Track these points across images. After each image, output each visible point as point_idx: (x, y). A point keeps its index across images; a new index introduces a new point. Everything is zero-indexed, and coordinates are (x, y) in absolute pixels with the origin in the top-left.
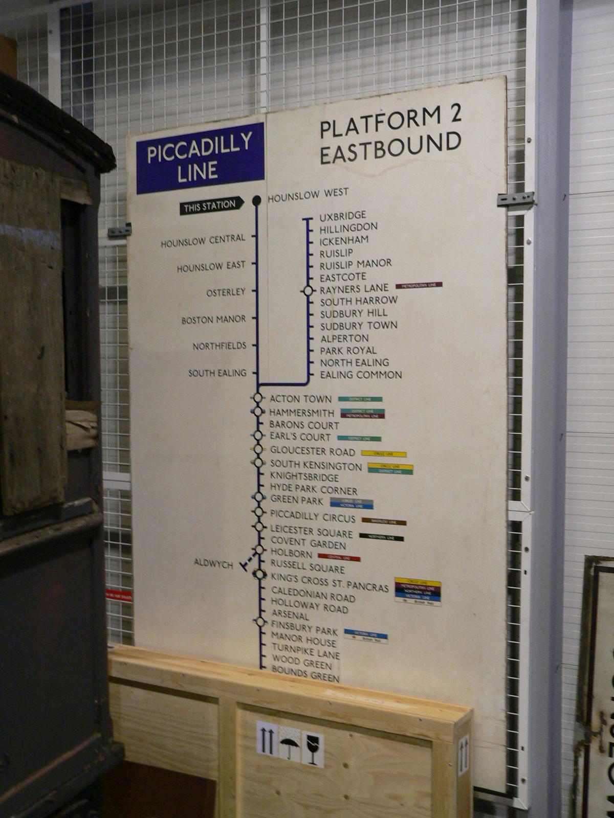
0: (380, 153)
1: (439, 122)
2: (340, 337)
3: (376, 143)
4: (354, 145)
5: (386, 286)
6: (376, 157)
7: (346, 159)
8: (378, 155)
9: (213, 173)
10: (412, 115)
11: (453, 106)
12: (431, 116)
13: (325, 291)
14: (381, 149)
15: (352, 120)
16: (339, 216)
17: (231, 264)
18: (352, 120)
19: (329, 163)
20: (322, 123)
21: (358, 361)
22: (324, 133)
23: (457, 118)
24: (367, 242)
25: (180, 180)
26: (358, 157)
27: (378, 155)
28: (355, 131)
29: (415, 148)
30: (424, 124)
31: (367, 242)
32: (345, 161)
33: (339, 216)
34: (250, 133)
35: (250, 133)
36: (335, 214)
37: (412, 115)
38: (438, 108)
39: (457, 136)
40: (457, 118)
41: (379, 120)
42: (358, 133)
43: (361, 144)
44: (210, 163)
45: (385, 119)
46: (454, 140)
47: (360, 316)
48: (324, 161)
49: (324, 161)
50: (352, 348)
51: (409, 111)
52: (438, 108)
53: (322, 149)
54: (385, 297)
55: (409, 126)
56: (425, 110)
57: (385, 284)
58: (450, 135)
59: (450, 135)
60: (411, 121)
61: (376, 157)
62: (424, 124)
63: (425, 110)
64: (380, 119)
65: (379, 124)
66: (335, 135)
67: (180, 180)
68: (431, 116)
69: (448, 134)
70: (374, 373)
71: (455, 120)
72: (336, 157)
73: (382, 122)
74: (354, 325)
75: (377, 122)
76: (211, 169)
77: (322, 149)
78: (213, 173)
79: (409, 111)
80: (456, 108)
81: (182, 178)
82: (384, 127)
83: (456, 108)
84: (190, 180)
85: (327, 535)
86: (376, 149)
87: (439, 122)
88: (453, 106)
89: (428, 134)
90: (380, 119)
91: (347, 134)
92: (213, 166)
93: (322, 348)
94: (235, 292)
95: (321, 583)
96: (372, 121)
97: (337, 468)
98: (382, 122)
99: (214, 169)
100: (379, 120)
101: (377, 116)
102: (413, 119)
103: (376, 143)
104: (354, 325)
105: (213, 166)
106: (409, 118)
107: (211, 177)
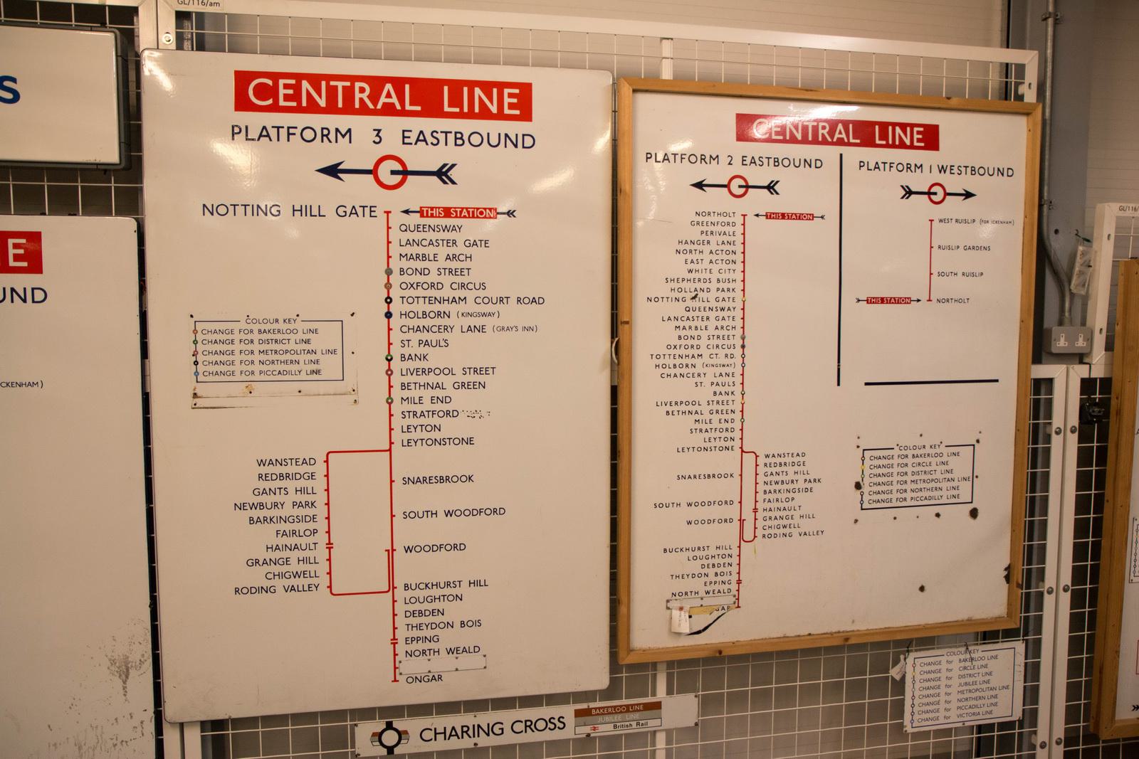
1: (350, 142)
3: (526, 721)
5: (373, 209)
6: (456, 145)
7: (429, 143)
8: (458, 143)
13: (418, 415)
14: (461, 138)
15: (877, 163)
17: (748, 160)
18: (877, 163)
19: (411, 144)
20: (647, 154)
21: (744, 159)
24: (922, 172)
25: (447, 109)
26: (439, 144)
27: (458, 143)
30: (336, 142)
31: (922, 172)
32: (427, 144)
36: (972, 167)
38: (717, 156)
41: (405, 135)
42: (459, 738)
43: (441, 132)
48: (405, 142)
49: (405, 142)
50: (457, 255)
52: (717, 156)
53: (404, 131)
54: (496, 146)
55: (12, 301)
57: (951, 166)
60: (325, 138)
61: (456, 145)
62: (336, 142)
63: (337, 130)
64: (292, 131)
65: (290, 136)
67: (447, 109)
70: (714, 157)
73: (294, 134)
74: (275, 505)
75: (433, 414)
77: (404, 131)
80: (730, 158)
81: (450, 106)
83: (730, 158)
84: (466, 110)
85: (406, 230)
86: (456, 139)
87: (350, 142)
91: (416, 144)
93: (861, 162)
95: (552, 726)
96: (887, 166)
97: (271, 213)
98: (294, 134)
100: (405, 135)
102: (327, 136)
104: (275, 505)
106: (323, 135)
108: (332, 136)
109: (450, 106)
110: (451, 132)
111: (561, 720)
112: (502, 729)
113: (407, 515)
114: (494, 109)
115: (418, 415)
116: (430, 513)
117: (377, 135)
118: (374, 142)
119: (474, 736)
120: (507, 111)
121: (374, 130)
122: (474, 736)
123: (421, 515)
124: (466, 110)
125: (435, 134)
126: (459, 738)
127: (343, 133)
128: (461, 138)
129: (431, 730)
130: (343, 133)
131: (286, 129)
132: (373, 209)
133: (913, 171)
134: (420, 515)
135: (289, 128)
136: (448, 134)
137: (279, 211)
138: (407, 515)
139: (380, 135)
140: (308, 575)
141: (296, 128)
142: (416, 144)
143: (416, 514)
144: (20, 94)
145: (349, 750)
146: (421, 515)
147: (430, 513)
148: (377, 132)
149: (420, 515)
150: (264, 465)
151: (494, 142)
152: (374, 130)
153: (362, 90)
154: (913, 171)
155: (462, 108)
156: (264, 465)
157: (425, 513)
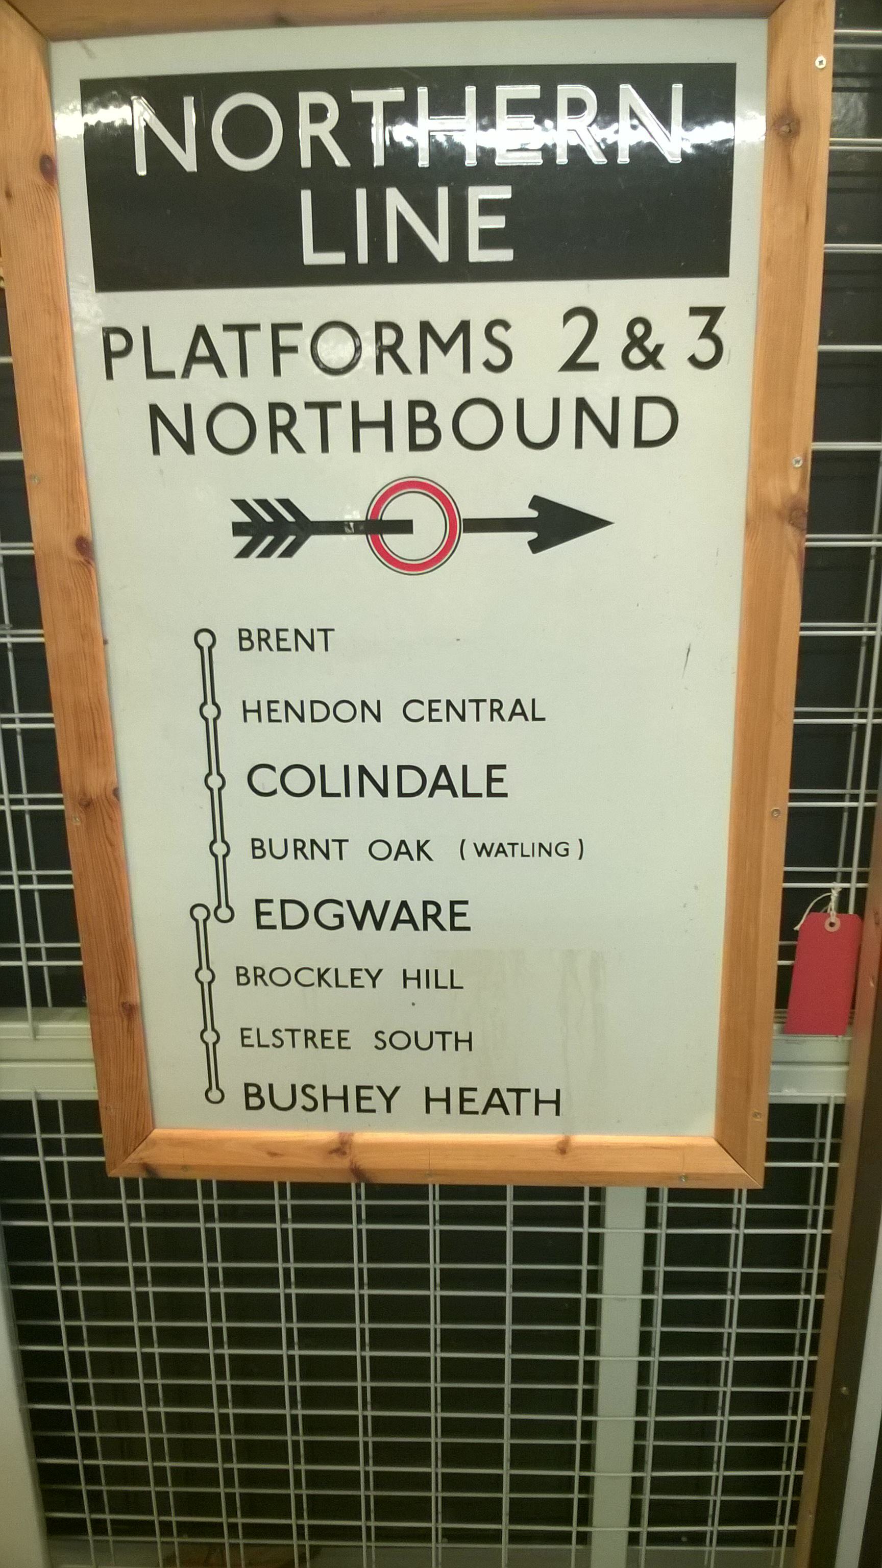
0: (424, 436)
2: (273, 706)
3: (492, 701)
4: (280, 1031)
8: (419, 441)
9: (488, 239)
10: (389, 337)
11: (568, 316)
12: (445, 348)
13: (506, 712)
16: (255, 638)
18: (201, 332)
21: (496, 774)
22: (115, 362)
23: (582, 360)
25: (311, 257)
27: (419, 441)
28: (212, 366)
29: (538, 430)
30: (424, 368)
33: (255, 638)
34: (379, 160)
35: (379, 160)
37: (432, 910)
39: (546, 439)
40: (582, 360)
44: (476, 194)
45: (302, 339)
46: (656, 421)
47: (389, 1110)
51: (273, 407)
56: (426, 328)
58: (646, 407)
59: (646, 407)
60: (430, 921)
62: (424, 368)
63: (426, 328)
64: (285, 338)
66: (151, 374)
67: (311, 257)
68: (445, 348)
69: (640, 401)
71: (572, 365)
72: (489, 1105)
73: (293, 349)
75: (278, 350)
76: (477, 222)
78: (488, 239)
79: (273, 407)
80: (580, 324)
81: (319, 247)
82: (297, 365)
83: (580, 324)
84: (363, 257)
88: (568, 316)
89: (191, 456)
90: (285, 338)
92: (487, 207)
94: (345, 979)
98: (293, 349)
99: (498, 222)
100: (282, 343)
101: (276, 328)
103: (492, 701)
105: (487, 207)
107: (476, 254)
108: (410, 351)
109: (319, 247)
110: (450, 1033)
111: (498, 332)
112: (567, 850)
113: (386, 1038)
114: (440, 250)
115: (506, 712)
116: (450, 1039)
117: (707, 333)
118: (693, 360)
119: (347, 795)
120: (476, 254)
121: (694, 311)
122: (347, 795)
123: (424, 1041)
124: (363, 257)
125: (277, 1033)
126: (416, 928)
127: (445, 339)
128: (430, 423)
129: (422, 703)
130: (445, 339)
131: (266, 333)
132: (496, 774)
133: (309, 855)
134: (424, 1043)
135: (276, 328)
136: (248, 335)
137: (567, 850)
138: (386, 1038)
139: (716, 330)
140: (253, 1040)
141: (298, 326)
142: (510, 719)
143: (413, 1040)
144: (463, 143)
145: (65, 1159)
146: (424, 1041)
147: (450, 1039)
148: (704, 320)
149: (424, 1043)
150: (378, 925)
151: (538, 433)
152: (694, 311)
153: (318, 114)
154: (309, 855)
155: (352, 253)
156: (378, 925)
157: (438, 1039)
